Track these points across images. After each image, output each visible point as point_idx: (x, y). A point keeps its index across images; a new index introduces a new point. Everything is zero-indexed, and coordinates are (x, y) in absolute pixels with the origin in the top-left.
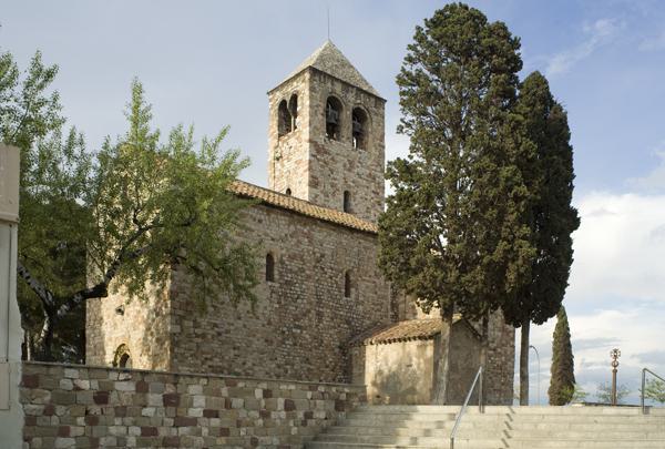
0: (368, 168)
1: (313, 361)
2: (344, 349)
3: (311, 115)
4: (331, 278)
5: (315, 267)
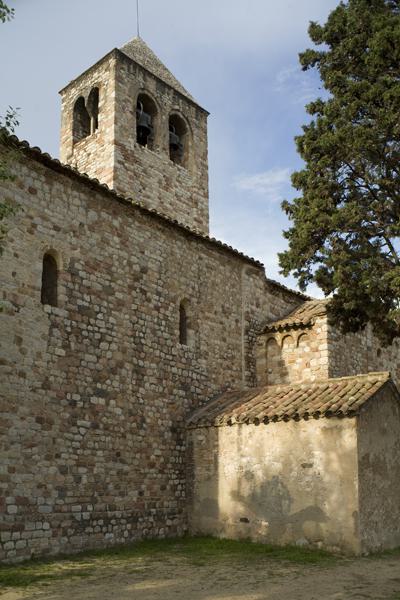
1: (127, 455)
2: (179, 432)
4: (157, 308)
5: (132, 288)
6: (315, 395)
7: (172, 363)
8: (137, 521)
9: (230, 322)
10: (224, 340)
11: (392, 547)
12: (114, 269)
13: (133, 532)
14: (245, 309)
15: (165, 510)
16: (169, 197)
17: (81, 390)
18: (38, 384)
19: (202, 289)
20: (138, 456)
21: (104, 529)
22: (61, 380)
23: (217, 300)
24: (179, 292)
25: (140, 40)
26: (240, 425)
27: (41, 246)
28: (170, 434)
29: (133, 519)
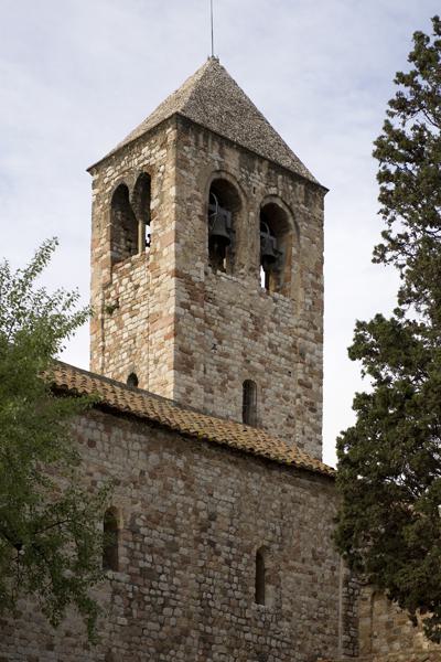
0: (290, 331)
3: (178, 218)
4: (228, 562)
5: (199, 540)
7: (246, 628)
19: (285, 532)
22: (124, 652)
24: (255, 538)
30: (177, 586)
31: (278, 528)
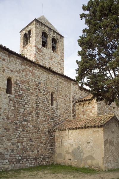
4: (44, 95)
5: (35, 89)
6: (92, 121)
8: (37, 160)
9: (67, 99)
10: (65, 104)
11: (116, 168)
12: (30, 83)
13: (35, 163)
14: (72, 95)
15: (46, 156)
16: (52, 62)
17: (19, 119)
18: (5, 118)
19: (58, 89)
20: (37, 140)
21: (26, 162)
22: (12, 117)
23: (63, 92)
24: (51, 90)
25: (43, 16)
26: (69, 130)
27: (6, 76)
28: (48, 133)
29: (36, 159)
30: (29, 100)
31: (56, 88)
